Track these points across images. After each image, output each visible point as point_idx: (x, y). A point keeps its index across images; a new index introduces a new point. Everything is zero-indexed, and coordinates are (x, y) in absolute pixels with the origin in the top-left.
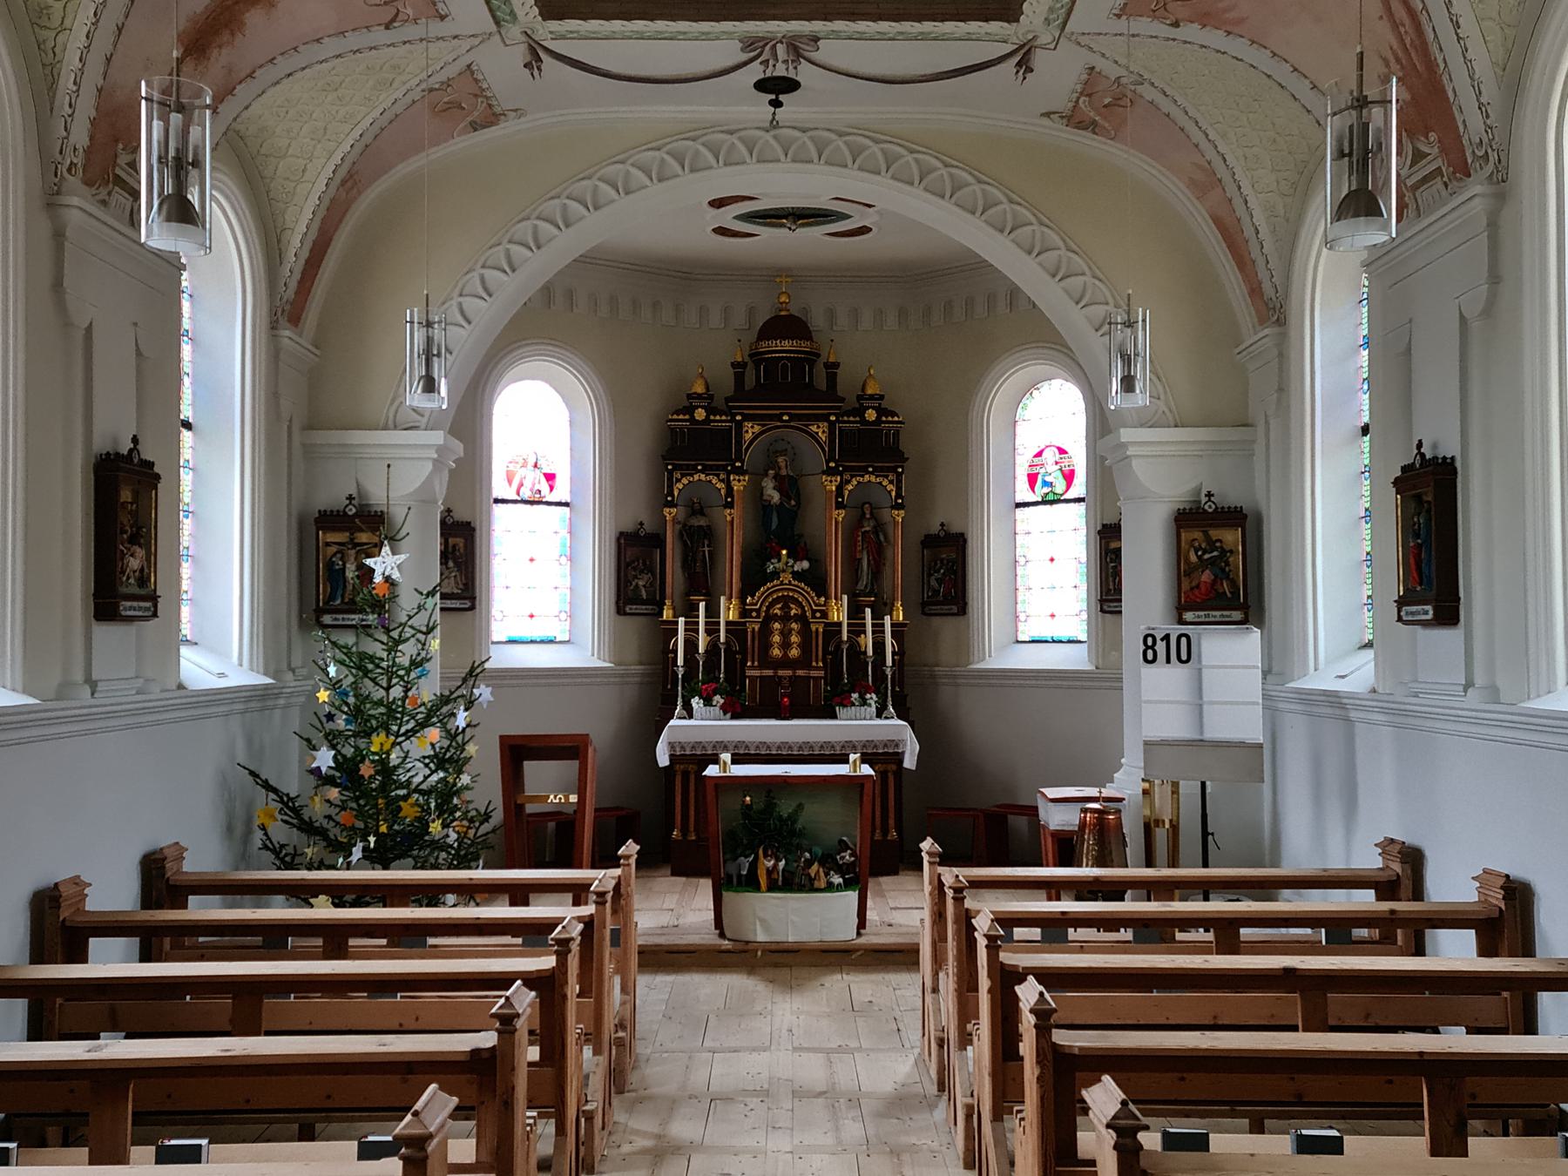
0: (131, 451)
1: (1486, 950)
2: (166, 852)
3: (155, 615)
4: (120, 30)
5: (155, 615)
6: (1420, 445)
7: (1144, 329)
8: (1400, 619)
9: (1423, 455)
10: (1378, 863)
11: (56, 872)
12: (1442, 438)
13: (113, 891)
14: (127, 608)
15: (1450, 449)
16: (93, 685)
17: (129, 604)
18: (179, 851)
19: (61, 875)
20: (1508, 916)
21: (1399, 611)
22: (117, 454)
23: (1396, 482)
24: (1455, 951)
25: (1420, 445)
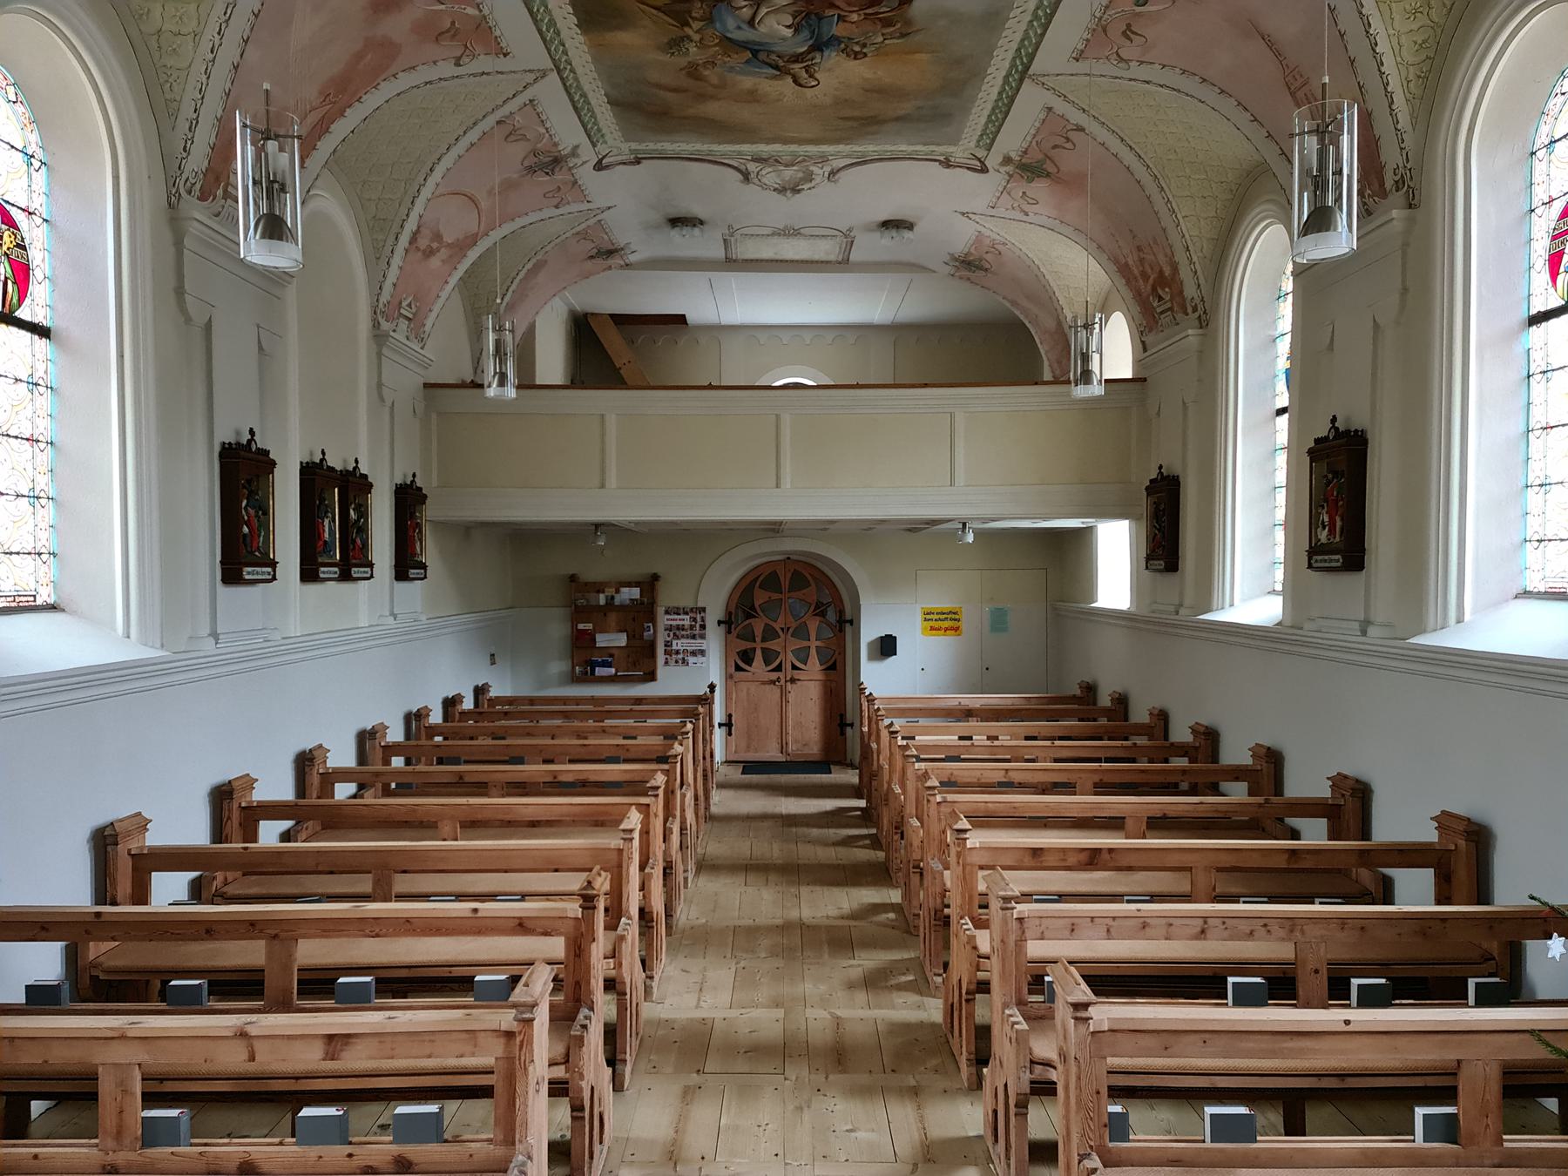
0: (249, 442)
1: (1333, 835)
2: (235, 784)
3: (274, 578)
4: (236, 68)
5: (274, 578)
6: (1334, 419)
7: (1350, 132)
8: (1310, 566)
9: (1337, 429)
10: (1250, 761)
11: (113, 810)
12: (1355, 415)
13: (277, 786)
14: (355, 572)
15: (1177, 470)
16: (215, 635)
17: (1334, 564)
18: (248, 782)
19: (309, 746)
20: (1463, 854)
21: (1310, 559)
22: (238, 444)
23: (1310, 452)
24: (1314, 834)
25: (1334, 419)
